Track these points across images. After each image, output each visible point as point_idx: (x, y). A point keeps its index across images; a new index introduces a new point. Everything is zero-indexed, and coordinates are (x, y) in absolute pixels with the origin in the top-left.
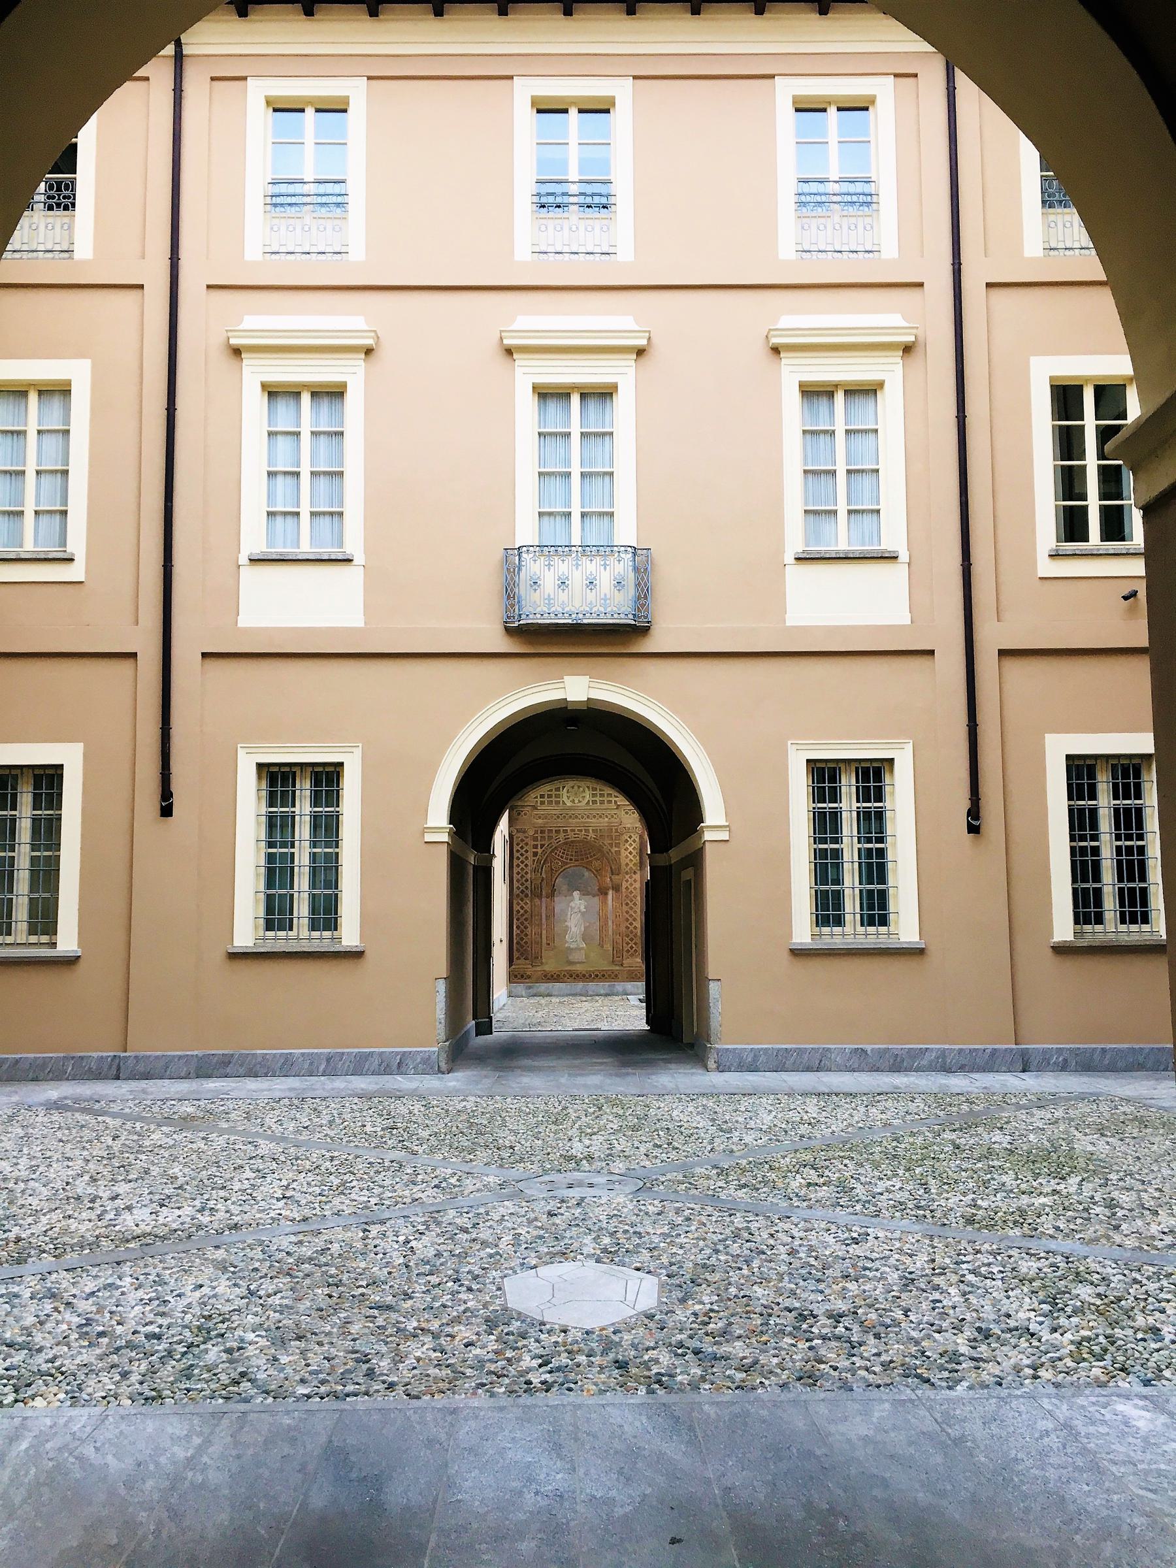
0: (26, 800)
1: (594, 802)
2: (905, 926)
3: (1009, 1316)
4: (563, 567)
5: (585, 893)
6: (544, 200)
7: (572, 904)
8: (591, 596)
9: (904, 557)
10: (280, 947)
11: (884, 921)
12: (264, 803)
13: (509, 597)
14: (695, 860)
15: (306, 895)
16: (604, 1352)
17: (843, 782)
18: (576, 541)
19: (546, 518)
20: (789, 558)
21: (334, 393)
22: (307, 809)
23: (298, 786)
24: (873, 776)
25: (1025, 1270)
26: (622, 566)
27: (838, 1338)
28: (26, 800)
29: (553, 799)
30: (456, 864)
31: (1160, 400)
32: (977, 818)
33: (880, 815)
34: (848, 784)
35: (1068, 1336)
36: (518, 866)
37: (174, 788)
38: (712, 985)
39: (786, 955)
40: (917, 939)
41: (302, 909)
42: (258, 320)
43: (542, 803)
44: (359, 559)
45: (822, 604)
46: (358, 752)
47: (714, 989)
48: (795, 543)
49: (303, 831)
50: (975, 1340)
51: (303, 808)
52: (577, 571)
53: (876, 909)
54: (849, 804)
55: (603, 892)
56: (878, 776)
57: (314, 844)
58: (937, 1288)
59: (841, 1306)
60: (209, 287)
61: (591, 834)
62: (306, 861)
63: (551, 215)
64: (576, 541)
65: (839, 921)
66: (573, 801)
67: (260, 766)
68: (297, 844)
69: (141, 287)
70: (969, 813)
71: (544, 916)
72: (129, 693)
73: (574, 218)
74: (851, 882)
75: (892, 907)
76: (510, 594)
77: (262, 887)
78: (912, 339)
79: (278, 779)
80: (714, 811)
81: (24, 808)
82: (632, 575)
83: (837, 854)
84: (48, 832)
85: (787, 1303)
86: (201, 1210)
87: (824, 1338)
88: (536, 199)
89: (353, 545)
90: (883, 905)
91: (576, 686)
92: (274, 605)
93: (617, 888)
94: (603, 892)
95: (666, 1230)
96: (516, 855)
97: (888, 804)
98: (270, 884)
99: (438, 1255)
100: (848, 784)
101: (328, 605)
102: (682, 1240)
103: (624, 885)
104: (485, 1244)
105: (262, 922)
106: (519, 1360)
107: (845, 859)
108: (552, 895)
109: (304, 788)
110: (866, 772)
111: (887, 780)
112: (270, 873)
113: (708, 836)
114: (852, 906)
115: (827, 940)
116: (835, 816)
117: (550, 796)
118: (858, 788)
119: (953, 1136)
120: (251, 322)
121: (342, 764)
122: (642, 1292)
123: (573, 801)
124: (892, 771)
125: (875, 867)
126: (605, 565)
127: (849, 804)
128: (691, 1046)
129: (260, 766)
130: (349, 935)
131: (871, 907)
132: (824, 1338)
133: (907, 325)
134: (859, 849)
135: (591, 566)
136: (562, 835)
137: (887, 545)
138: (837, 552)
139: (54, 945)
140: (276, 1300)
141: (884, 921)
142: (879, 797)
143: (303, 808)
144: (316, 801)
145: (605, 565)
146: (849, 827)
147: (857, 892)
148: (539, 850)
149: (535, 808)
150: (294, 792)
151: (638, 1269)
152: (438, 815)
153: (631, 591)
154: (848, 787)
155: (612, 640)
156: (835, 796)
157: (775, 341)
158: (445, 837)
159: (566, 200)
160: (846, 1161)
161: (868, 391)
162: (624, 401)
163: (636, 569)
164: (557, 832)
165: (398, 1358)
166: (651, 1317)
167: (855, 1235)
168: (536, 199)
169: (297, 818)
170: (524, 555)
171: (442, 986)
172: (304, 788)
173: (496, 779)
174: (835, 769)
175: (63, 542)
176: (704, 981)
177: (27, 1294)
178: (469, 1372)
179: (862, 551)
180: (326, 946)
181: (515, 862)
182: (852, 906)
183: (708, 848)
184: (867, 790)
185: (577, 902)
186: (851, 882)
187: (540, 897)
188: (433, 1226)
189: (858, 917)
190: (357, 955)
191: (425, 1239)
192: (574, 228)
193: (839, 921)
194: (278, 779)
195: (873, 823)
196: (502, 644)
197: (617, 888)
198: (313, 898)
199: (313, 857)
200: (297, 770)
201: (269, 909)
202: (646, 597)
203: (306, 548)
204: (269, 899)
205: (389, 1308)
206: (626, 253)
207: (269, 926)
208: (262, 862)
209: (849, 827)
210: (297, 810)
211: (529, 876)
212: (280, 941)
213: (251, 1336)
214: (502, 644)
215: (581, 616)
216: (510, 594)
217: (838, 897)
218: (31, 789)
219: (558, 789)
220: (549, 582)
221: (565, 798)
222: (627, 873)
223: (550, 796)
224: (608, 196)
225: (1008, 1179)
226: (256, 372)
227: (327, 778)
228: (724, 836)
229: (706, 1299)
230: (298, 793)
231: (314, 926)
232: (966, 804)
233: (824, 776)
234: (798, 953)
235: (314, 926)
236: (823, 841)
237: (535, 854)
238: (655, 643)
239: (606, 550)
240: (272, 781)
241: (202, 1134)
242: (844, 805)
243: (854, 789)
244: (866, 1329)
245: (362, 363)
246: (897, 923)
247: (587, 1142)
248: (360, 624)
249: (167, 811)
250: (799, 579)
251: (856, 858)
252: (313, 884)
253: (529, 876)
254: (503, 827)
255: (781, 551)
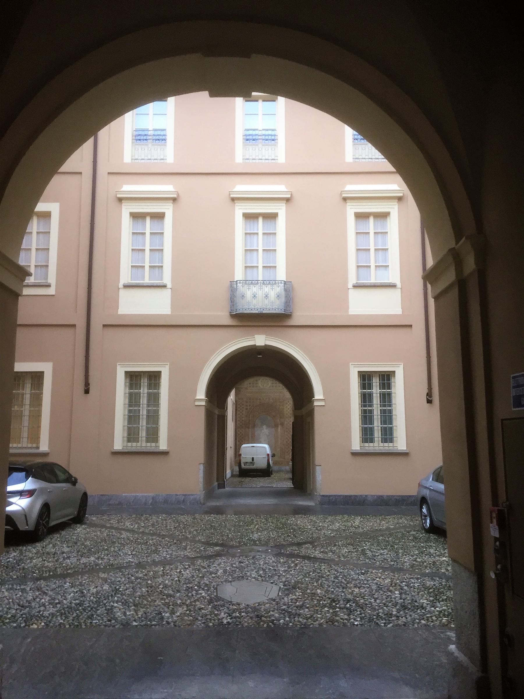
0: (28, 386)
1: (272, 386)
2: (401, 443)
3: (416, 601)
4: (255, 289)
5: (268, 426)
6: (248, 137)
7: (263, 431)
8: (266, 302)
9: (399, 285)
10: (133, 449)
11: (391, 441)
12: (128, 389)
13: (232, 302)
14: (311, 413)
15: (145, 428)
16: (253, 612)
17: (374, 381)
18: (260, 278)
19: (248, 269)
20: (350, 286)
21: (159, 217)
22: (146, 391)
23: (142, 381)
24: (386, 378)
25: (428, 585)
26: (279, 289)
27: (347, 608)
28: (28, 386)
29: (255, 385)
30: (209, 414)
31: (439, 258)
32: (431, 396)
33: (389, 394)
34: (376, 382)
35: (438, 609)
36: (239, 414)
37: (91, 381)
38: (317, 468)
39: (350, 455)
40: (405, 449)
41: (143, 434)
42: (129, 188)
43: (250, 386)
44: (169, 285)
45: (363, 305)
46: (167, 367)
47: (318, 470)
48: (352, 280)
49: (144, 401)
50: (400, 610)
51: (144, 390)
52: (259, 291)
53: (388, 435)
54: (376, 391)
55: (276, 426)
56: (389, 379)
57: (148, 406)
58: (391, 591)
59: (349, 596)
60: (109, 173)
61: (271, 401)
62: (145, 413)
63: (251, 144)
64: (260, 278)
65: (372, 441)
66: (263, 386)
67: (126, 372)
68: (141, 405)
69: (81, 173)
70: (427, 394)
71: (250, 436)
72: (71, 342)
73: (260, 145)
74: (377, 424)
75: (395, 435)
76: (232, 300)
77: (126, 424)
78: (402, 195)
79: (133, 378)
80: (318, 394)
81: (27, 389)
82: (283, 292)
83: (371, 412)
84: (37, 400)
85: (329, 596)
86: (98, 558)
87: (340, 608)
88: (245, 137)
89: (167, 279)
90: (391, 434)
91: (260, 340)
92: (133, 305)
93: (282, 424)
94: (276, 426)
95: (286, 569)
96: (238, 409)
97: (393, 390)
98: (129, 422)
99: (193, 576)
100: (376, 382)
101: (156, 305)
102: (292, 572)
103: (286, 423)
104: (211, 573)
105: (126, 439)
106: (219, 615)
107: (375, 414)
108: (254, 426)
109: (145, 382)
110: (383, 376)
111: (393, 380)
112: (130, 417)
113: (316, 404)
114: (377, 434)
115: (387, 448)
116: (370, 395)
117: (253, 384)
118: (380, 383)
119: (415, 533)
120: (126, 188)
121: (160, 372)
122: (274, 591)
123: (263, 386)
124: (394, 376)
125: (387, 417)
126: (272, 289)
127: (376, 391)
128: (310, 494)
129: (126, 372)
130: (163, 446)
131: (386, 434)
132: (340, 608)
133: (399, 189)
134: (381, 410)
135: (267, 289)
136: (258, 401)
137: (391, 281)
138: (371, 283)
139: (38, 448)
140: (127, 592)
141: (391, 441)
142: (389, 388)
143: (144, 390)
144: (150, 387)
145: (272, 289)
146: (376, 400)
147: (380, 428)
148: (248, 407)
149: (246, 389)
150: (140, 384)
151: (272, 583)
152: (201, 394)
153: (283, 300)
154: (376, 384)
155: (275, 320)
156: (370, 387)
157: (344, 195)
158: (203, 403)
159: (257, 137)
160: (367, 543)
161: (384, 216)
162: (281, 220)
163: (286, 290)
164: (257, 399)
165: (173, 613)
166: (274, 600)
167: (363, 571)
168: (245, 137)
169: (142, 395)
170: (238, 284)
171: (202, 467)
172: (145, 382)
173: (231, 374)
174: (370, 375)
175: (46, 278)
176: (314, 466)
177: (28, 589)
178: (200, 618)
179: (381, 283)
180: (153, 449)
181: (238, 412)
182: (377, 434)
183: (316, 408)
184: (384, 384)
185: (265, 430)
186: (377, 424)
187: (249, 428)
188: (191, 566)
189: (380, 439)
190: (165, 453)
191: (188, 571)
192: (260, 149)
193: (372, 441)
194: (133, 378)
195: (387, 399)
196: (228, 321)
197: (282, 424)
198: (147, 428)
199: (148, 411)
200: (142, 374)
201: (129, 434)
202: (290, 302)
203: (147, 281)
204: (129, 429)
205: (171, 596)
206: (282, 159)
207: (129, 440)
208: (127, 413)
209: (376, 400)
210: (141, 391)
211: (244, 419)
212: (134, 446)
213: (116, 605)
214: (228, 321)
215: (262, 310)
216: (232, 300)
217: (372, 430)
218: (30, 381)
219: (257, 381)
220: (249, 294)
221: (260, 385)
222: (287, 418)
223: (253, 384)
224: (275, 135)
225: (432, 551)
226: (126, 209)
227: (154, 378)
228: (322, 403)
229: (297, 594)
230: (142, 384)
231: (147, 441)
232: (426, 391)
233: (365, 378)
234: (355, 454)
235: (147, 441)
236: (365, 406)
237: (247, 409)
238: (296, 320)
239: (272, 282)
240: (131, 380)
241: (100, 529)
242: (374, 391)
243: (378, 384)
244: (358, 605)
245: (172, 205)
246: (397, 441)
247: (260, 534)
248: (170, 313)
249: (87, 392)
250: (354, 296)
251: (379, 413)
252: (148, 423)
253: (244, 419)
254: (232, 397)
255: (346, 282)
